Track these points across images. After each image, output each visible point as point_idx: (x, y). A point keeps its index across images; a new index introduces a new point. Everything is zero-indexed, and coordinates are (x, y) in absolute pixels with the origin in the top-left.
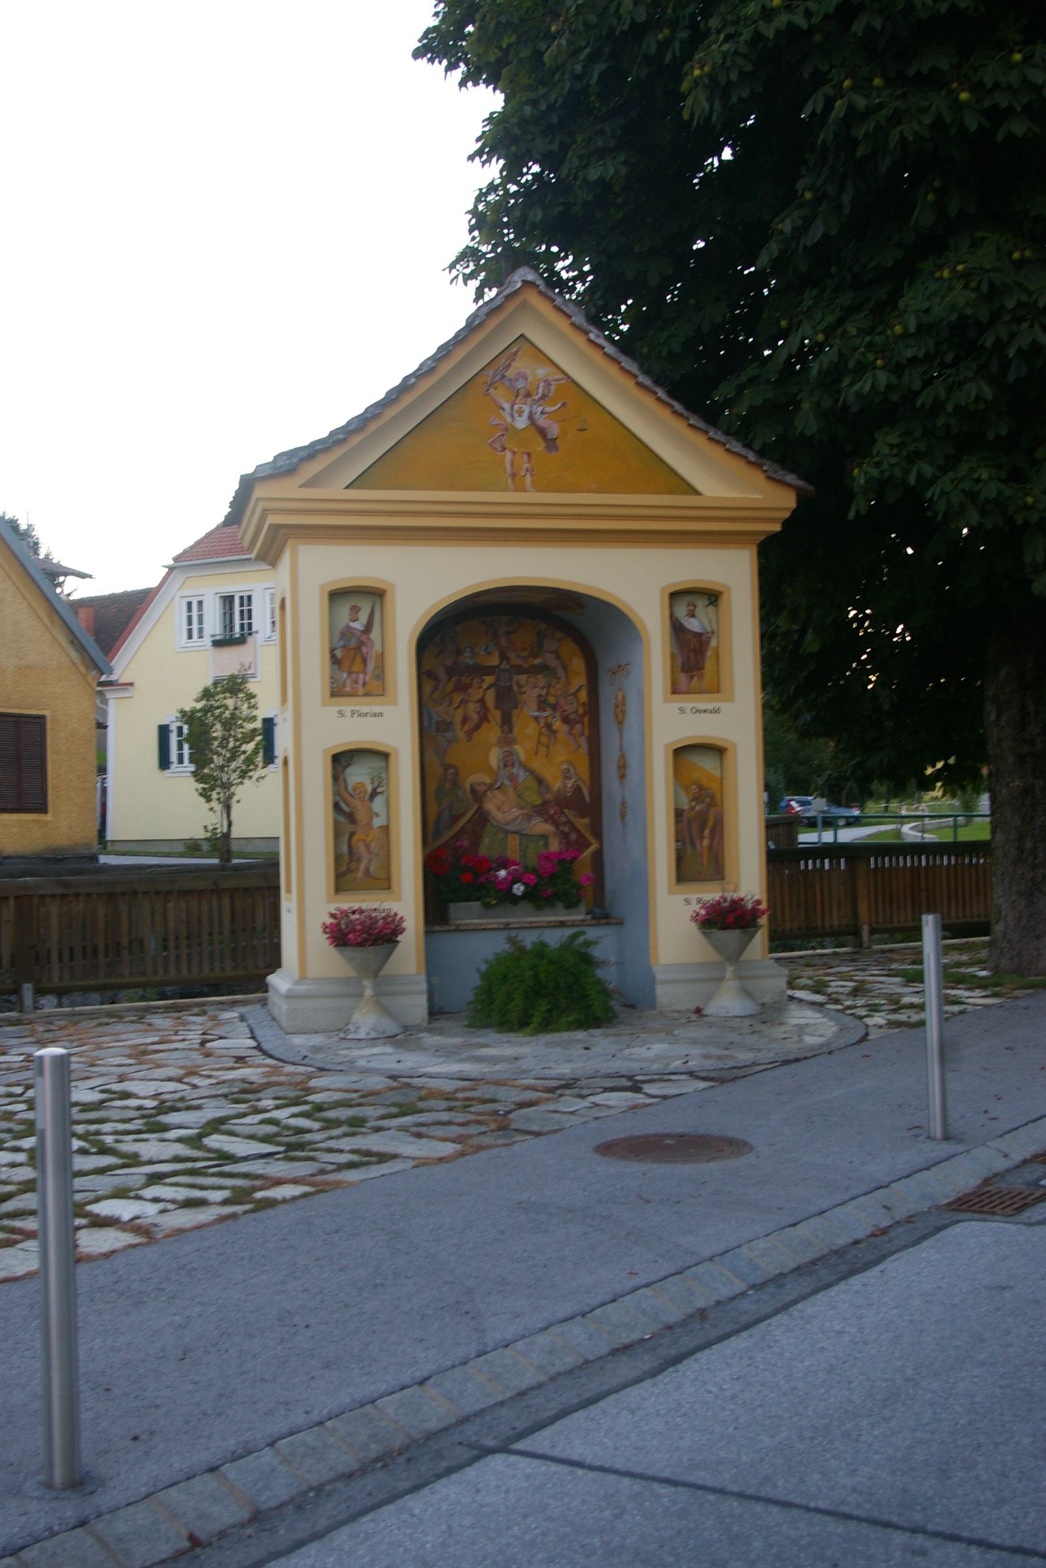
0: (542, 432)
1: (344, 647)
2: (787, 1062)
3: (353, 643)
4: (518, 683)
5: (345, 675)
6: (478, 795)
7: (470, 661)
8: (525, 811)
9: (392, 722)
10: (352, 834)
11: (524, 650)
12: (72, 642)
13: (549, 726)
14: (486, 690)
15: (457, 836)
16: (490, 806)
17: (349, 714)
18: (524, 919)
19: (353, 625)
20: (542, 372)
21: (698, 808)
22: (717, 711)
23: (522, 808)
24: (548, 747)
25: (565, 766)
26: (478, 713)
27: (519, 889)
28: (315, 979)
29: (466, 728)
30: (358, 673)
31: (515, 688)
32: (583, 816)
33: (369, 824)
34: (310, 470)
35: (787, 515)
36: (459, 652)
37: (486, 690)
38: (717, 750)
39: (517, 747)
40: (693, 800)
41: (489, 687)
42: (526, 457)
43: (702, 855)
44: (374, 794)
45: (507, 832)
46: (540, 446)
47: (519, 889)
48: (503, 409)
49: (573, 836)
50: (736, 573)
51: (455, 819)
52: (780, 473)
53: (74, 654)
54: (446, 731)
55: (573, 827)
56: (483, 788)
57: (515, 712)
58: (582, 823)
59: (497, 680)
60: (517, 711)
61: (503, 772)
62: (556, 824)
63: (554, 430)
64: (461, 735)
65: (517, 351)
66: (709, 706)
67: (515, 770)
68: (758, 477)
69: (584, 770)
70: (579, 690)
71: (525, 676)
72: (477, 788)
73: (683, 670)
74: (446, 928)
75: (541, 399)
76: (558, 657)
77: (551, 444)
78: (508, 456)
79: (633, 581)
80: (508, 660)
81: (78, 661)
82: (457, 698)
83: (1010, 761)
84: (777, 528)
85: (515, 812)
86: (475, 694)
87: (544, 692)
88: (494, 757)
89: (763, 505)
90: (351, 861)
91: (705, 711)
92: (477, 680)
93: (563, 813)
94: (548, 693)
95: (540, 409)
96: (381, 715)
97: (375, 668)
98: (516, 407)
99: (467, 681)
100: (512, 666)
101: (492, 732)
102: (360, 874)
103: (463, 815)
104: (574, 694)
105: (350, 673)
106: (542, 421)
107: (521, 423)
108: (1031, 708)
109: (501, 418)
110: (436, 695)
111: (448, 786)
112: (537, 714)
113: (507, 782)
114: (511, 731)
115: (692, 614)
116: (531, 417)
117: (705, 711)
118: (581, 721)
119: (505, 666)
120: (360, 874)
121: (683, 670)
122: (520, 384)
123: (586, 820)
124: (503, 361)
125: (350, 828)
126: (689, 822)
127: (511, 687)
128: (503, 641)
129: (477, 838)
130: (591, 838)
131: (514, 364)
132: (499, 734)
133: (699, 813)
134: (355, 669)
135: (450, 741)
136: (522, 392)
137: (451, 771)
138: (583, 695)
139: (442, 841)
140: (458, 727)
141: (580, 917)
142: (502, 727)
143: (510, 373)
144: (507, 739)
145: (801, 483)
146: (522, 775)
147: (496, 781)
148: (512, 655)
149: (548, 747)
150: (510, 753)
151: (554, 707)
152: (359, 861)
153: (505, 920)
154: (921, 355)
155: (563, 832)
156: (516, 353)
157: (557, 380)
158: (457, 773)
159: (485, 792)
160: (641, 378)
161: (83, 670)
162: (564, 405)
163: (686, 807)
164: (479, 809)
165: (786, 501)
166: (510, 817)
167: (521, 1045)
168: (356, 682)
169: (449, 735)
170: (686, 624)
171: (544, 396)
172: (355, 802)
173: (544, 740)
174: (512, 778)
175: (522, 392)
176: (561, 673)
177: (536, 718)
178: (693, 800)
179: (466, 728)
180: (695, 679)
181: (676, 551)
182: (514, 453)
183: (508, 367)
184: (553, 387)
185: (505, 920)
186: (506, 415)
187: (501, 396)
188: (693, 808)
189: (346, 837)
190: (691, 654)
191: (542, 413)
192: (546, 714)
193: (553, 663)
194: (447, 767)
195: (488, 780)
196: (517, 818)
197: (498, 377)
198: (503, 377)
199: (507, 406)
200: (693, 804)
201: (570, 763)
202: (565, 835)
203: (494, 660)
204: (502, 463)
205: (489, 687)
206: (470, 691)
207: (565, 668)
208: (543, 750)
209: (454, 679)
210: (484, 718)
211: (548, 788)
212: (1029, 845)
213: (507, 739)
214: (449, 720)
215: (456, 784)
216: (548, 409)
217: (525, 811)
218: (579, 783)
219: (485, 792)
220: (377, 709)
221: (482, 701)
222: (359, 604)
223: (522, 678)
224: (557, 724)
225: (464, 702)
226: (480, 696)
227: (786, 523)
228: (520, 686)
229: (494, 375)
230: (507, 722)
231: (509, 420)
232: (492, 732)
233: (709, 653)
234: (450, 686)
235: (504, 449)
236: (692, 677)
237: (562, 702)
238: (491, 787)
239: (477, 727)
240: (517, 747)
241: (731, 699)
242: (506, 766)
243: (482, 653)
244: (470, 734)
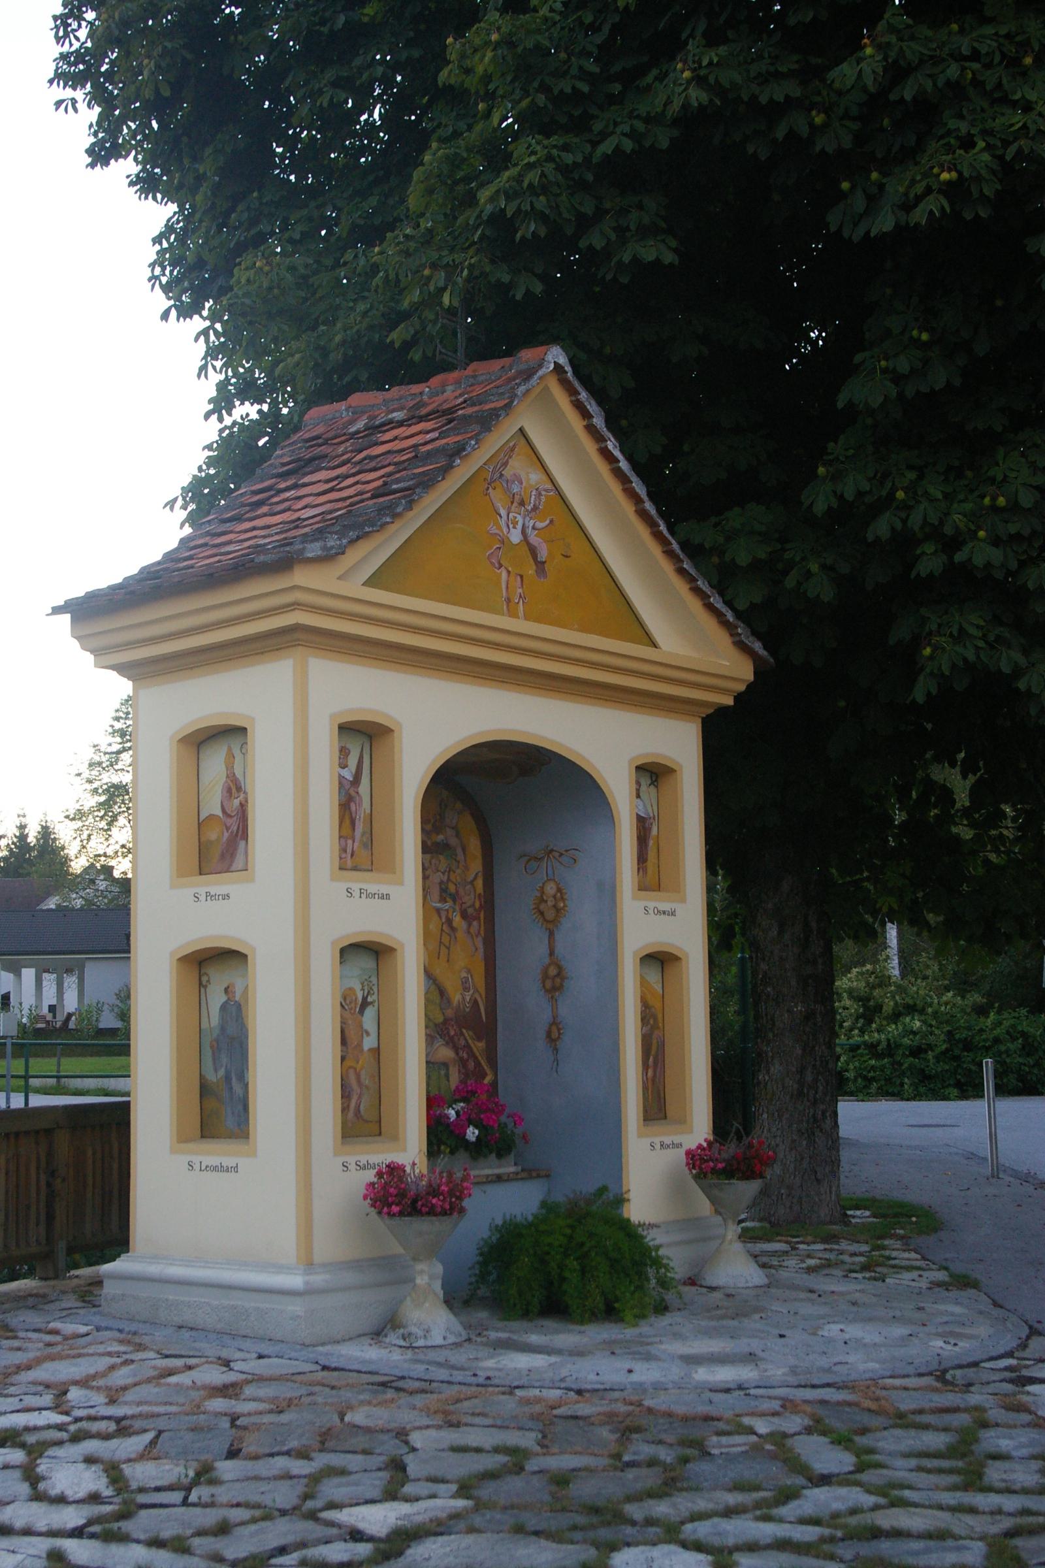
0: (533, 551)
9: (396, 909)
13: (449, 922)
20: (535, 478)
24: (448, 948)
25: (464, 974)
27: (472, 1133)
28: (324, 1265)
32: (479, 1039)
33: (360, 1045)
35: (742, 688)
44: (365, 1004)
47: (472, 1133)
49: (471, 1064)
50: (681, 744)
52: (751, 639)
55: (472, 1055)
58: (479, 1046)
62: (456, 1049)
68: (723, 639)
69: (480, 981)
70: (475, 878)
76: (457, 835)
77: (540, 566)
78: (504, 575)
79: (605, 742)
83: (794, 983)
84: (729, 701)
87: (445, 878)
89: (727, 673)
91: (664, 913)
93: (462, 1034)
94: (449, 880)
97: (363, 834)
104: (472, 882)
106: (534, 539)
107: (515, 537)
108: (814, 925)
109: (499, 528)
112: (438, 905)
117: (664, 913)
118: (477, 918)
122: (515, 489)
123: (481, 1045)
130: (488, 1071)
136: (517, 498)
138: (479, 883)
141: (512, 1169)
149: (448, 948)
151: (454, 898)
154: (1026, 532)
155: (461, 1059)
160: (649, 506)
162: (551, 521)
165: (741, 671)
167: (557, 1332)
171: (535, 508)
173: (446, 939)
176: (460, 857)
177: (438, 911)
181: (629, 714)
182: (509, 572)
183: (506, 464)
184: (543, 499)
186: (503, 523)
187: (497, 496)
191: (534, 528)
192: (447, 906)
193: (453, 841)
198: (501, 475)
199: (503, 512)
201: (469, 971)
202: (463, 1063)
207: (464, 850)
208: (444, 950)
211: (449, 1001)
212: (809, 1077)
218: (477, 996)
222: (348, 746)
224: (457, 920)
227: (739, 698)
231: (505, 530)
233: (651, 843)
235: (501, 566)
237: (461, 892)
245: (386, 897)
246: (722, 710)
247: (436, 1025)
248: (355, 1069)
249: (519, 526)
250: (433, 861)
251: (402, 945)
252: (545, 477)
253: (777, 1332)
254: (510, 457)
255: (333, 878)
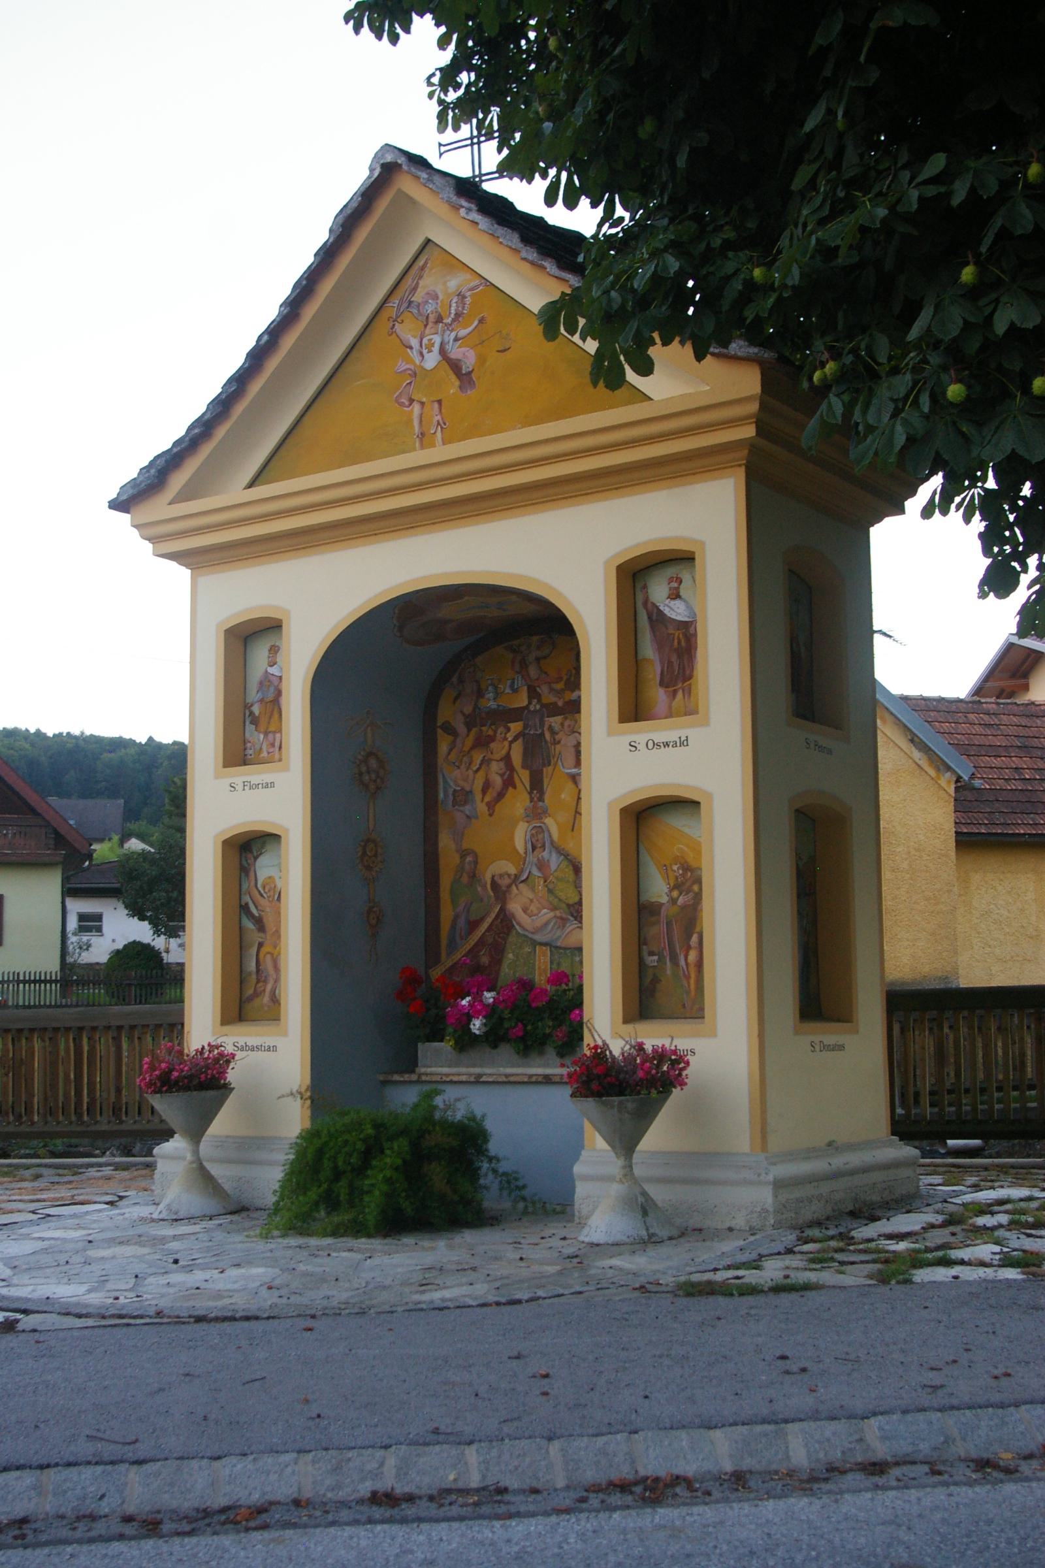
0: (455, 366)
1: (261, 701)
2: (199, 1319)
3: (271, 695)
4: (551, 728)
5: (262, 736)
6: (500, 892)
7: (492, 704)
8: (558, 913)
10: (261, 945)
11: (560, 679)
12: (912, 741)
14: (511, 742)
15: (473, 952)
16: (515, 907)
17: (239, 787)
18: (509, 1071)
19: (270, 670)
21: (680, 901)
22: (684, 743)
23: (554, 909)
26: (502, 775)
29: (487, 798)
30: (275, 732)
31: (548, 736)
34: (178, 480)
35: (754, 407)
36: (480, 694)
37: (511, 742)
38: (685, 805)
39: (549, 821)
40: (676, 887)
41: (515, 739)
42: (436, 405)
43: (688, 978)
45: (535, 943)
46: (452, 385)
48: (411, 348)
51: (473, 925)
53: (917, 755)
54: (466, 802)
56: (506, 881)
57: (547, 771)
59: (526, 727)
60: (550, 768)
61: (531, 858)
63: (468, 357)
64: (482, 807)
65: (426, 263)
66: (672, 736)
67: (545, 854)
71: (559, 719)
72: (499, 881)
73: (661, 684)
74: (406, 1077)
75: (454, 320)
77: (465, 379)
78: (416, 408)
79: (565, 558)
80: (538, 697)
81: (924, 763)
82: (478, 757)
84: (749, 431)
85: (546, 915)
86: (498, 749)
88: (520, 836)
89: (703, 403)
90: (258, 981)
91: (667, 745)
92: (501, 729)
95: (453, 335)
96: (272, 785)
98: (425, 341)
99: (490, 732)
100: (543, 706)
101: (518, 801)
102: (266, 999)
103: (482, 920)
105: (266, 734)
106: (455, 352)
107: (431, 360)
109: (409, 360)
110: (453, 755)
111: (465, 879)
113: (535, 872)
114: (541, 799)
115: (675, 595)
116: (442, 351)
117: (667, 745)
119: (536, 706)
120: (266, 999)
121: (661, 684)
122: (430, 308)
124: (409, 281)
125: (257, 937)
126: (669, 924)
127: (542, 734)
128: (533, 671)
129: (498, 952)
131: (421, 283)
132: (527, 803)
133: (684, 907)
134: (272, 728)
135: (468, 817)
137: (469, 859)
139: (458, 955)
140: (478, 797)
142: (530, 793)
143: (418, 297)
144: (536, 813)
145: (754, 350)
146: (554, 861)
147: (522, 871)
148: (544, 690)
150: (540, 829)
152: (265, 981)
153: (477, 1070)
156: (423, 268)
157: (472, 289)
158: (476, 863)
159: (509, 886)
161: (932, 772)
162: (481, 321)
163: (664, 899)
164: (502, 910)
166: (539, 921)
168: (273, 745)
169: (467, 809)
170: (667, 611)
172: (263, 902)
174: (542, 866)
175: (432, 318)
178: (676, 887)
179: (487, 798)
180: (680, 695)
181: (607, 504)
182: (423, 404)
183: (415, 289)
184: (468, 300)
185: (477, 1070)
186: (414, 355)
188: (674, 901)
189: (254, 950)
190: (674, 658)
191: (456, 339)
194: (464, 854)
195: (512, 870)
196: (546, 924)
197: (405, 305)
198: (410, 302)
199: (414, 342)
200: (675, 894)
203: (522, 700)
204: (409, 421)
205: (515, 739)
206: (492, 745)
209: (474, 730)
210: (509, 783)
213: (536, 813)
214: (468, 789)
215: (473, 876)
216: (463, 333)
217: (558, 913)
219: (509, 886)
220: (267, 778)
221: (507, 759)
223: (555, 721)
225: (486, 762)
226: (504, 752)
228: (553, 732)
229: (399, 306)
230: (537, 786)
231: (417, 360)
232: (518, 801)
234: (469, 742)
235: (411, 401)
236: (675, 693)
238: (516, 879)
239: (501, 796)
240: (549, 821)
241: (705, 722)
242: (534, 848)
243: (508, 690)
244: (491, 806)
245: (269, 785)
246: (752, 447)
247: (569, 906)
248: (272, 954)
249: (436, 349)
250: (567, 723)
251: (287, 831)
252: (468, 276)
253: (181, 1263)
254: (421, 277)
255: (217, 776)
